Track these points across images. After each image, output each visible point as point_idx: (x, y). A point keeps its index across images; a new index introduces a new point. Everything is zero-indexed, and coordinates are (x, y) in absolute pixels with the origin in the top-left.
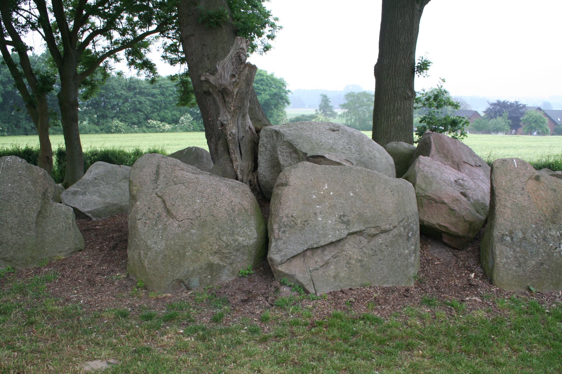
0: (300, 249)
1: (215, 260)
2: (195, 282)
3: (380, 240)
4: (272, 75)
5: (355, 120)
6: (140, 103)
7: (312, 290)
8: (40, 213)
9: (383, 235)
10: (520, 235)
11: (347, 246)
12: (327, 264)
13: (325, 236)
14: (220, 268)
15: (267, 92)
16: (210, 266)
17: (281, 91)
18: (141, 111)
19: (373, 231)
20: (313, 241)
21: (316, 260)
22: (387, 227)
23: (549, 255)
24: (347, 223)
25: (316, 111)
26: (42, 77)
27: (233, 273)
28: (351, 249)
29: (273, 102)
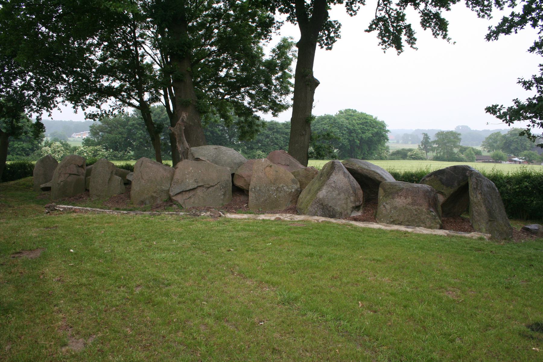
0: (179, 191)
1: (154, 195)
2: (147, 202)
3: (210, 189)
4: (376, 118)
5: (444, 153)
6: (277, 139)
7: (184, 207)
8: (110, 179)
9: (212, 188)
10: (258, 188)
11: (198, 191)
12: (190, 197)
13: (188, 186)
14: (156, 198)
15: (370, 132)
16: (152, 197)
17: (382, 130)
18: (277, 145)
19: (207, 186)
20: (184, 188)
21: (187, 195)
22: (213, 184)
23: (270, 197)
24: (197, 182)
25: (419, 146)
26: (158, 125)
27: (161, 200)
28: (199, 192)
29: (375, 139)
